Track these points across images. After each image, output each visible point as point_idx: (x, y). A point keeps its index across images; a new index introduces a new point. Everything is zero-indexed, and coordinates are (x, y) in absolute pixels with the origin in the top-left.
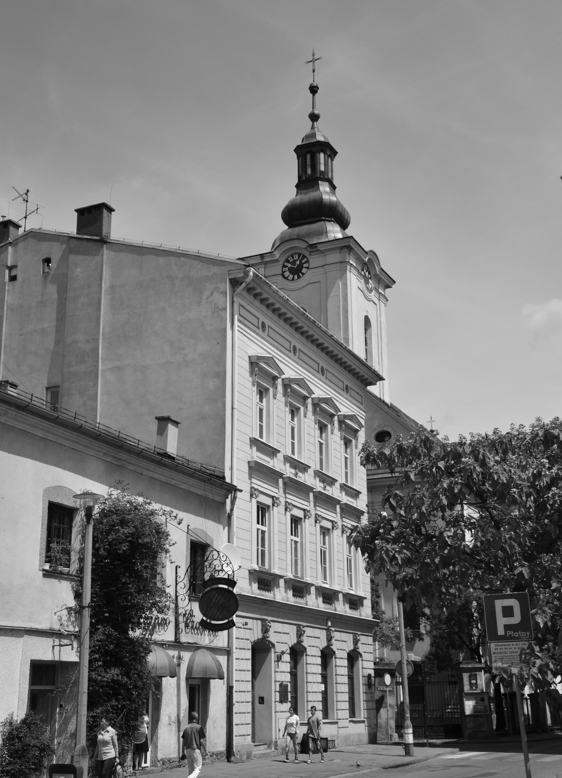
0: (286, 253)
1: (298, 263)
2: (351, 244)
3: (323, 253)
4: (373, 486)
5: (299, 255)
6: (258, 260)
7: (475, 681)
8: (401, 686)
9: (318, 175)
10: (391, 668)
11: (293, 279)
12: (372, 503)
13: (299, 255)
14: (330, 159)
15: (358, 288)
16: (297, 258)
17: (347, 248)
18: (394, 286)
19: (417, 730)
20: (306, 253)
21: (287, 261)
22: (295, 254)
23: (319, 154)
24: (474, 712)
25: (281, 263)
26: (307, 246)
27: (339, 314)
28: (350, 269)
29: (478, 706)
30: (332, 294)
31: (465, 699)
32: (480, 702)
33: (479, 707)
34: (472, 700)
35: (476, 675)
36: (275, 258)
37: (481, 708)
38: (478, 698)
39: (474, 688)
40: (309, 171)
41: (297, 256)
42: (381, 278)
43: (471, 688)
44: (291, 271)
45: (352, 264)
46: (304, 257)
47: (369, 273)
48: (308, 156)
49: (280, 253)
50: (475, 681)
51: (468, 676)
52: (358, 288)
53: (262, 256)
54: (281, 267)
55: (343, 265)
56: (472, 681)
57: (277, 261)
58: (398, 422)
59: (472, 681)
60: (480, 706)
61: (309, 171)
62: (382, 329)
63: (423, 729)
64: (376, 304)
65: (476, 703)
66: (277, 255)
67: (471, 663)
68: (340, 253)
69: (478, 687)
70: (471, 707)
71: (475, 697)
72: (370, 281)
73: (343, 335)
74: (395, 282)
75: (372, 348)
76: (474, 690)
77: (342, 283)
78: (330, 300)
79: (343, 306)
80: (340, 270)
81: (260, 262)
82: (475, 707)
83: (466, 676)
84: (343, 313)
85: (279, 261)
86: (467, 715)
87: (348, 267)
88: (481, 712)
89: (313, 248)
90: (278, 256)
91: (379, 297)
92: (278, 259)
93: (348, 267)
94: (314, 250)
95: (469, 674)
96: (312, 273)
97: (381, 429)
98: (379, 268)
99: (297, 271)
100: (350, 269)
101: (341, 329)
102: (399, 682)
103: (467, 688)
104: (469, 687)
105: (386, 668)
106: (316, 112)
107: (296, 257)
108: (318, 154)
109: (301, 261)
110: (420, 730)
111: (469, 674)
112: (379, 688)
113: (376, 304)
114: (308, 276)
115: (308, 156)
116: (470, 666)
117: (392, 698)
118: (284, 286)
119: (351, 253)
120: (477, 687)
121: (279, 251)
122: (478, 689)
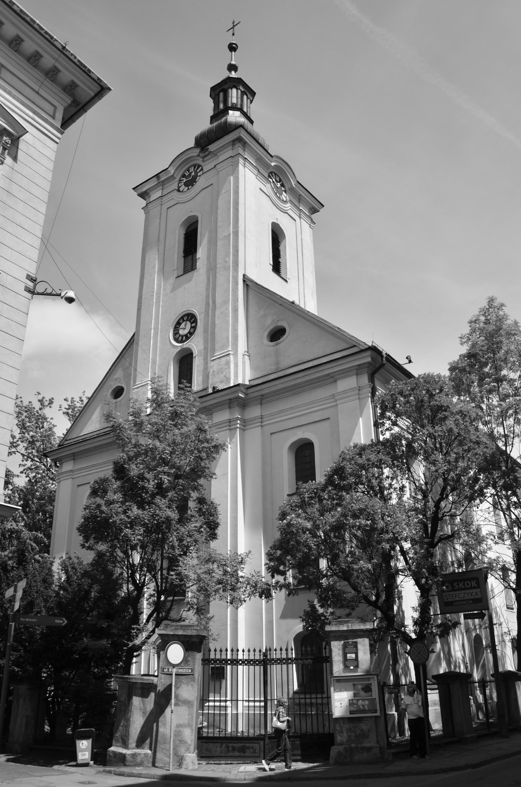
0: (182, 169)
1: (193, 174)
2: (242, 136)
3: (216, 155)
4: (262, 395)
5: (195, 166)
6: (154, 182)
7: (353, 656)
8: (294, 665)
9: (230, 105)
10: (189, 633)
11: (188, 189)
12: (262, 418)
13: (195, 166)
14: (245, 97)
15: (260, 189)
16: (192, 170)
17: (240, 142)
18: (322, 210)
19: (250, 745)
20: (199, 161)
21: (184, 176)
22: (190, 167)
23: (232, 89)
24: (351, 712)
25: (177, 179)
26: (198, 151)
27: (229, 209)
28: (245, 164)
29: (358, 700)
30: (223, 191)
31: (332, 689)
32: (362, 693)
33: (360, 702)
34: (346, 690)
35: (355, 645)
36: (170, 175)
37: (363, 704)
38: (360, 687)
39: (352, 668)
40: (221, 106)
41: (193, 168)
42: (300, 195)
43: (346, 667)
44: (187, 184)
45: (246, 158)
46: (199, 166)
47: (282, 185)
48: (221, 95)
49: (175, 169)
50: (353, 656)
51: (341, 647)
52: (260, 189)
53: (157, 176)
54: (177, 183)
55: (235, 159)
56: (348, 655)
57: (172, 177)
58: (294, 312)
59: (348, 655)
60: (363, 700)
61: (221, 106)
62: (305, 246)
63: (262, 743)
64: (295, 220)
65: (355, 695)
66: (172, 170)
67: (347, 622)
68: (230, 408)
69: (360, 665)
70: (345, 703)
71: (354, 685)
72: (284, 193)
73: (233, 229)
74: (323, 206)
75: (286, 260)
76: (351, 671)
77: (234, 178)
78: (221, 197)
79: (233, 200)
80: (230, 430)
81: (157, 184)
82: (351, 703)
83: (336, 647)
84: (234, 206)
85: (175, 178)
86: (337, 719)
87: (241, 161)
88: (364, 711)
89: (205, 152)
90: (172, 172)
91: (300, 215)
92: (173, 176)
93: (241, 161)
94: (207, 153)
95: (342, 642)
96: (205, 178)
97: (274, 325)
98: (296, 182)
99: (191, 182)
100: (245, 164)
101: (230, 223)
102: (290, 659)
103: (338, 668)
104: (341, 666)
105: (180, 632)
106: (233, 62)
107: (192, 170)
108: (230, 90)
109: (196, 172)
110: (256, 746)
111: (342, 642)
112: (166, 670)
113: (295, 220)
114: (201, 182)
115: (221, 95)
116: (345, 628)
117: (190, 688)
118: (179, 199)
119: (246, 149)
120: (357, 666)
121: (174, 167)
122: (359, 670)
